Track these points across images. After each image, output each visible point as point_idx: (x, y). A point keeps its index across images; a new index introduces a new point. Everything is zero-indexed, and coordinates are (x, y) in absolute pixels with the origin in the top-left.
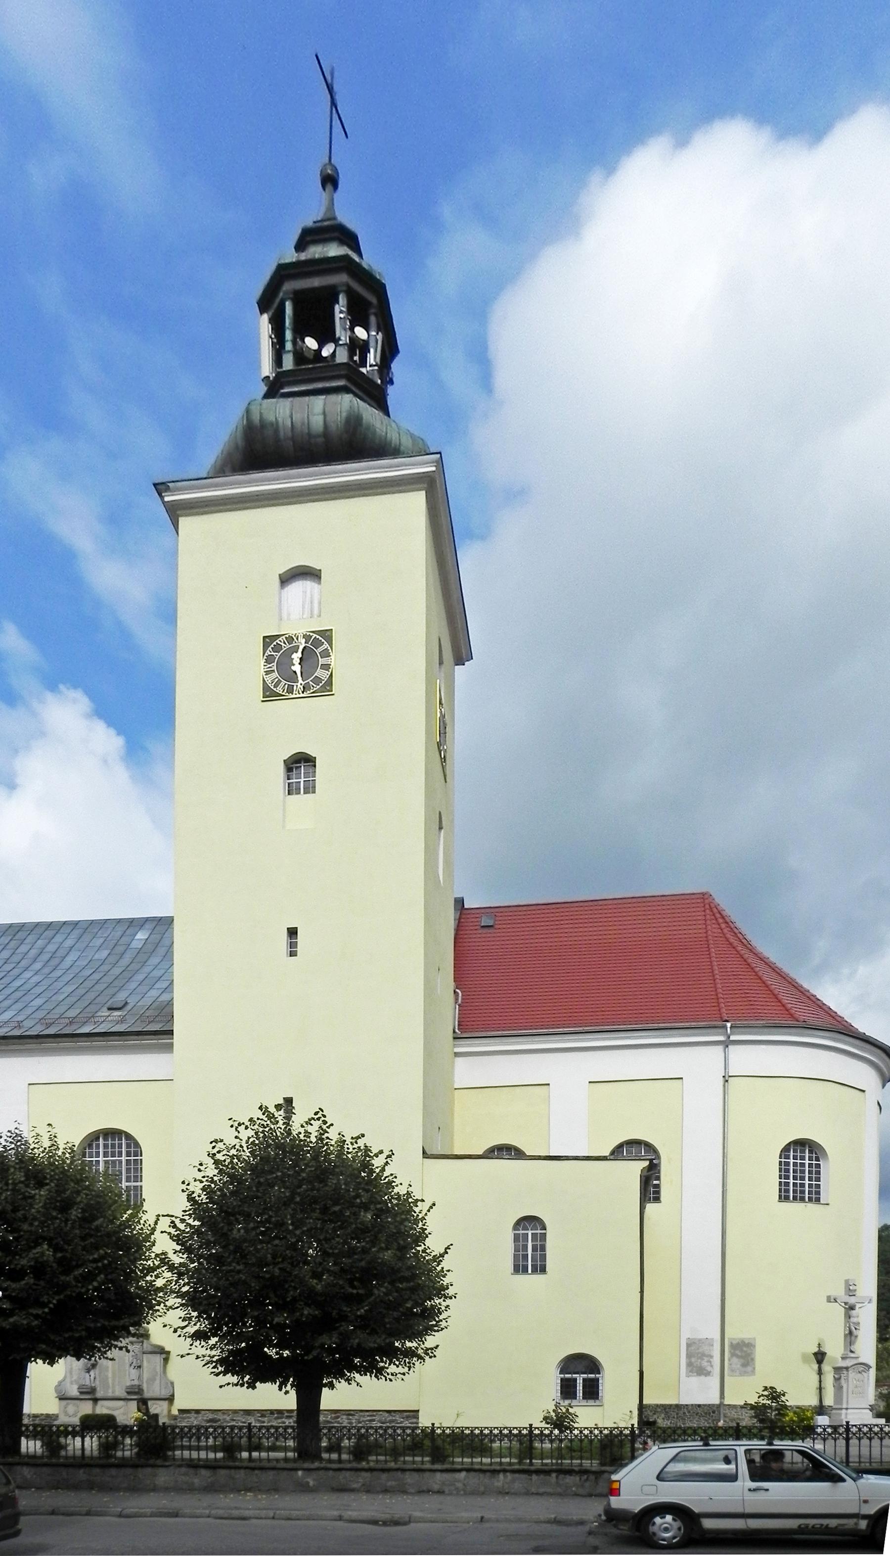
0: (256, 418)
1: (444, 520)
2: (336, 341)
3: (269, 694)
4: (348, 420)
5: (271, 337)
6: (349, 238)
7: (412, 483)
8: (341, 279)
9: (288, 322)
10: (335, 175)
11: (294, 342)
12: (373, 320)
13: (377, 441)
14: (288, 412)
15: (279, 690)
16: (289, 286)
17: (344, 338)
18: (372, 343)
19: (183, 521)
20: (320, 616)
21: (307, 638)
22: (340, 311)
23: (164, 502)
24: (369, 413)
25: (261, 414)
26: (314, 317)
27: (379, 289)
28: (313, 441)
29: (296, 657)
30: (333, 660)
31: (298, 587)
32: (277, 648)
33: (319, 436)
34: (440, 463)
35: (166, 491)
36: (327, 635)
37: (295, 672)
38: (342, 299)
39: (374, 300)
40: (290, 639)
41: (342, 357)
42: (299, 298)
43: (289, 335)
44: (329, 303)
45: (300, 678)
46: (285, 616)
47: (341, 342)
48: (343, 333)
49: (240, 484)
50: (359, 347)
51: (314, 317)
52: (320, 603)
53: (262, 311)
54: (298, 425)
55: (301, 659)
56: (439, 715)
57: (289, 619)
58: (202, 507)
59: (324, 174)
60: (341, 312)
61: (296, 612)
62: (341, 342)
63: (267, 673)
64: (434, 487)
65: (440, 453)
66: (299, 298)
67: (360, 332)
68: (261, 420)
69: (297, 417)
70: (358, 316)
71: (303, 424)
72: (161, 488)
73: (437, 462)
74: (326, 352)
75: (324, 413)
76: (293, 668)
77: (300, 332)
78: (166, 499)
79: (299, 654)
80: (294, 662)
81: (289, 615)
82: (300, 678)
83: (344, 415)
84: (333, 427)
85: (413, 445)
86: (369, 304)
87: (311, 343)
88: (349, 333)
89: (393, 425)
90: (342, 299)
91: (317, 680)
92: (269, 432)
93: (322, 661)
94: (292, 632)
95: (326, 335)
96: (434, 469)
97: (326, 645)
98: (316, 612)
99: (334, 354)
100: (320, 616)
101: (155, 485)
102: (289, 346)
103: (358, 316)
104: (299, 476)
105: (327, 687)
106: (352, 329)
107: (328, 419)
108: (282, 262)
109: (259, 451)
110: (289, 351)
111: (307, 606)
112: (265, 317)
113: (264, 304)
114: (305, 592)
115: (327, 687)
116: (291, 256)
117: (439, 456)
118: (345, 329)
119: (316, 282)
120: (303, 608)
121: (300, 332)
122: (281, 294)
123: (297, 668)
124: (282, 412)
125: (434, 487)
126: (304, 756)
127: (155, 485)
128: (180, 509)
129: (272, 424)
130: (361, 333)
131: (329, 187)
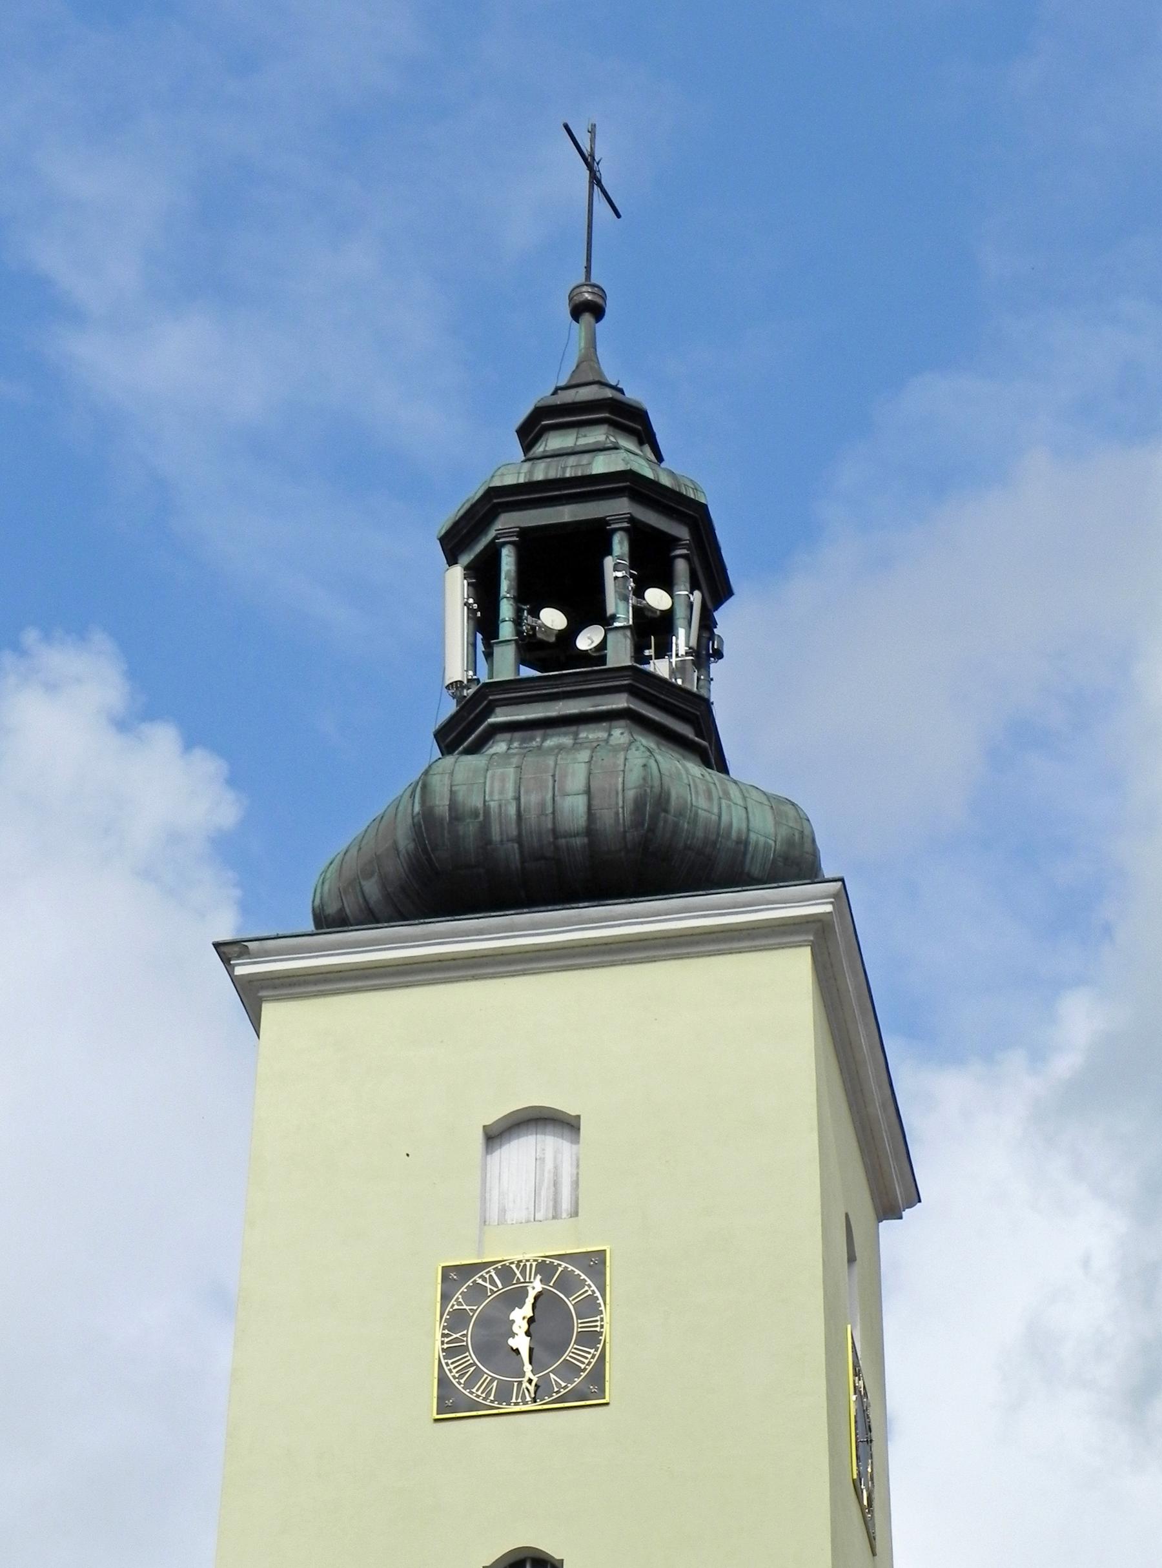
0: (441, 803)
1: (850, 983)
2: (606, 621)
3: (451, 1403)
4: (639, 805)
5: (466, 604)
6: (633, 422)
7: (784, 933)
8: (621, 507)
9: (505, 586)
10: (599, 300)
11: (518, 621)
12: (681, 567)
13: (700, 834)
14: (510, 793)
15: (476, 1393)
16: (508, 522)
17: (620, 609)
18: (680, 613)
19: (270, 1011)
20: (575, 1213)
21: (544, 1268)
22: (614, 570)
23: (235, 980)
24: (683, 774)
25: (452, 793)
26: (562, 567)
27: (697, 517)
28: (562, 842)
29: (520, 1316)
30: (609, 1322)
31: (524, 1149)
32: (478, 1292)
33: (577, 835)
34: (842, 898)
35: (238, 957)
36: (594, 1263)
37: (517, 1351)
38: (620, 545)
39: (682, 532)
40: (506, 1272)
41: (620, 654)
42: (529, 543)
43: (506, 610)
44: (589, 557)
45: (528, 1368)
46: (493, 1214)
47: (616, 624)
48: (622, 605)
49: (404, 941)
50: (653, 630)
51: (562, 567)
52: (576, 1184)
53: (452, 561)
54: (532, 817)
55: (531, 1321)
56: (854, 1398)
57: (502, 1221)
58: (316, 983)
59: (578, 299)
60: (616, 568)
61: (520, 1211)
62: (616, 624)
63: (450, 1352)
64: (834, 951)
65: (842, 880)
66: (529, 543)
67: (657, 598)
68: (453, 805)
69: (531, 799)
70: (651, 566)
71: (542, 813)
72: (228, 951)
73: (836, 896)
74: (587, 640)
75: (588, 792)
76: (512, 1342)
77: (531, 598)
78: (239, 971)
79: (527, 1311)
80: (515, 1328)
81: (503, 1211)
82: (528, 1368)
83: (631, 794)
84: (606, 819)
85: (777, 824)
86: (674, 541)
87: (553, 619)
88: (632, 600)
89: (734, 791)
90: (620, 545)
91: (571, 1370)
92: (470, 829)
93: (578, 1326)
94: (512, 1256)
95: (587, 608)
96: (829, 908)
97: (591, 1287)
98: (566, 1205)
99: (603, 645)
100: (575, 1213)
101: (217, 945)
102: (506, 631)
103: (651, 566)
104: (535, 926)
105: (590, 1389)
106: (639, 593)
107: (595, 802)
108: (497, 483)
109: (447, 878)
110: (518, 671)
111: (546, 1193)
112: (457, 571)
113: (454, 543)
114: (540, 1160)
115: (590, 1389)
116: (514, 469)
117: (840, 883)
118: (626, 599)
119: (566, 514)
120: (536, 1193)
121: (531, 598)
122: (492, 533)
123: (521, 1342)
124: (500, 785)
125: (834, 951)
126: (531, 1555)
127: (217, 945)
128: (262, 988)
129: (475, 814)
130: (657, 598)
131: (587, 318)
